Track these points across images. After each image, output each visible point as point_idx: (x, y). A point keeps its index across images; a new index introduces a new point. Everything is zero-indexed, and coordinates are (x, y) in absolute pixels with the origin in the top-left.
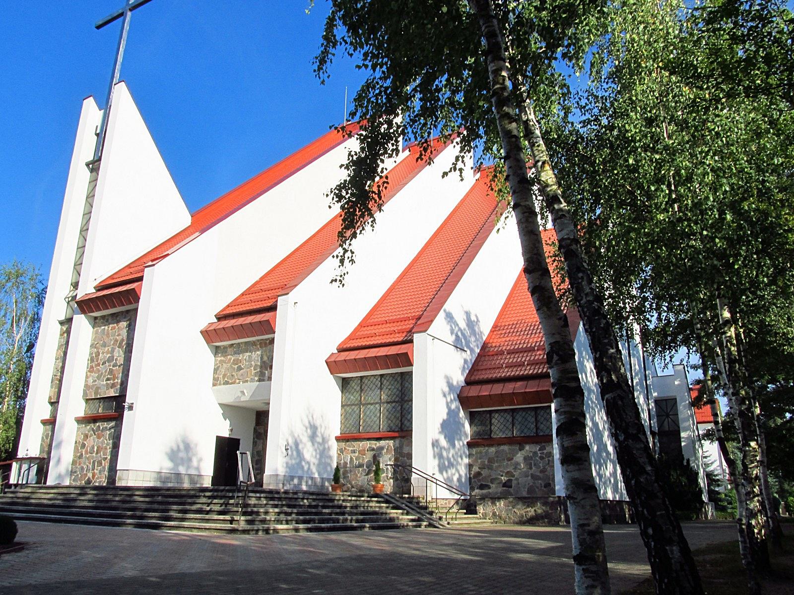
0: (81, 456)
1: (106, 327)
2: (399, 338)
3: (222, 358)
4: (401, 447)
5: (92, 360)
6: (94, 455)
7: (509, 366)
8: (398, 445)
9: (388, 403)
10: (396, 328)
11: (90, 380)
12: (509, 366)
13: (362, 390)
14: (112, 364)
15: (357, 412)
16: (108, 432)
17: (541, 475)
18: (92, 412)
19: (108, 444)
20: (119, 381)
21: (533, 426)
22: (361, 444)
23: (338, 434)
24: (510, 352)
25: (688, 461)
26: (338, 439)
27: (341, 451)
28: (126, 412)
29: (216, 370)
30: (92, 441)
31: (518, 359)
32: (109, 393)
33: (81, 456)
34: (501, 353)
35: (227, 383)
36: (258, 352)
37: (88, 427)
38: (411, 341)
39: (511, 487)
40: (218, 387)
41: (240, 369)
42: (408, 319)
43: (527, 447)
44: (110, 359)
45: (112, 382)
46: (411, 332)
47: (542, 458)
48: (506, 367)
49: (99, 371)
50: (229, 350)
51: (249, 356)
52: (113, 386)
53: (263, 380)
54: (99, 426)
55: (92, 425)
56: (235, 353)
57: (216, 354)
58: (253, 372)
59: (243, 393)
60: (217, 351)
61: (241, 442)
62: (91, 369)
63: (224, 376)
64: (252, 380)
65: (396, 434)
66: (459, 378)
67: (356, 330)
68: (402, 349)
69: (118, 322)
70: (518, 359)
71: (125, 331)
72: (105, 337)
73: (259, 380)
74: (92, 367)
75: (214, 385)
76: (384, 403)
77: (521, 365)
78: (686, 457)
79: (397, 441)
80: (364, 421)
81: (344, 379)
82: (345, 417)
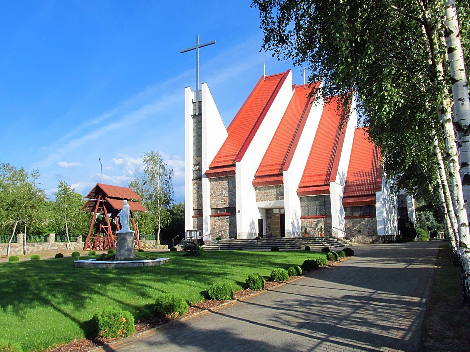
0: (214, 228)
1: (217, 182)
2: (277, 172)
3: (259, 192)
4: (326, 221)
5: (212, 194)
6: (221, 228)
7: (358, 191)
8: (325, 220)
9: (319, 205)
10: (312, 179)
11: (213, 202)
12: (358, 191)
13: (308, 201)
14: (223, 196)
15: (307, 209)
16: (226, 220)
17: (371, 228)
18: (215, 213)
19: (226, 224)
20: (228, 202)
21: (368, 212)
22: (310, 220)
23: (193, 215)
24: (357, 185)
25: (411, 219)
26: (211, 216)
27: (302, 222)
28: (237, 214)
29: (256, 196)
30: (218, 223)
31: (361, 188)
32: (222, 206)
33: (214, 228)
34: (353, 185)
35: (262, 201)
36: (275, 190)
37: (216, 218)
38: (329, 185)
39: (361, 232)
40: (257, 202)
41: (267, 196)
42: (277, 164)
43: (366, 219)
44: (221, 194)
45: (224, 202)
46: (281, 169)
47: (372, 222)
48: (357, 191)
49: (216, 198)
50: (261, 189)
51: (271, 191)
52: (225, 204)
53: (278, 200)
54: (221, 218)
55: (218, 218)
56: (264, 190)
57: (256, 190)
58: (273, 197)
59: (270, 204)
60: (256, 189)
61: (263, 220)
62: (212, 198)
63: (261, 198)
64: (273, 200)
65: (324, 216)
66: (342, 195)
67: (214, 160)
68: (277, 178)
69: (222, 180)
70: (361, 188)
71: (227, 184)
72: (217, 186)
73: (277, 200)
74: (212, 197)
75: (256, 201)
76: (318, 206)
77: (362, 190)
78: (410, 218)
79: (325, 219)
80: (310, 212)
81: (300, 197)
82: (302, 211)
